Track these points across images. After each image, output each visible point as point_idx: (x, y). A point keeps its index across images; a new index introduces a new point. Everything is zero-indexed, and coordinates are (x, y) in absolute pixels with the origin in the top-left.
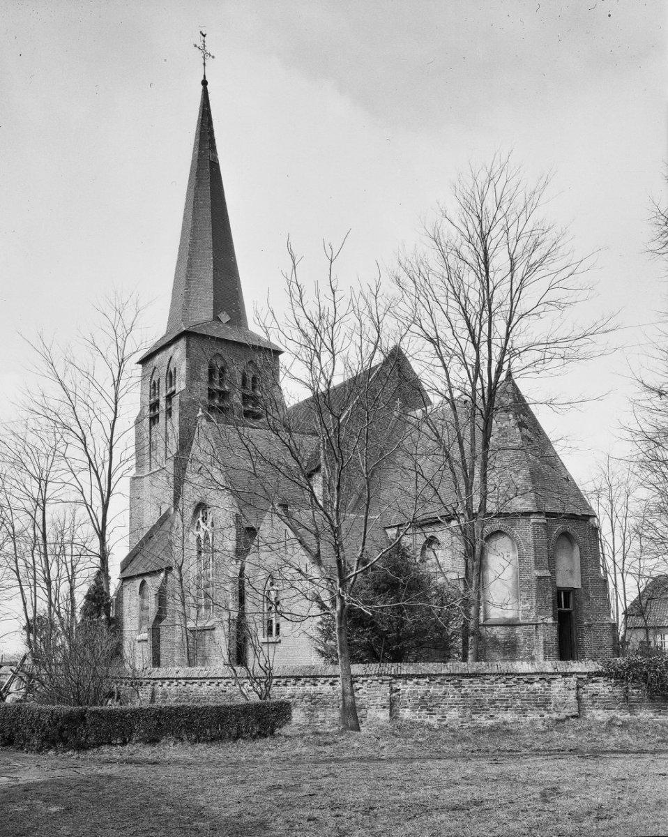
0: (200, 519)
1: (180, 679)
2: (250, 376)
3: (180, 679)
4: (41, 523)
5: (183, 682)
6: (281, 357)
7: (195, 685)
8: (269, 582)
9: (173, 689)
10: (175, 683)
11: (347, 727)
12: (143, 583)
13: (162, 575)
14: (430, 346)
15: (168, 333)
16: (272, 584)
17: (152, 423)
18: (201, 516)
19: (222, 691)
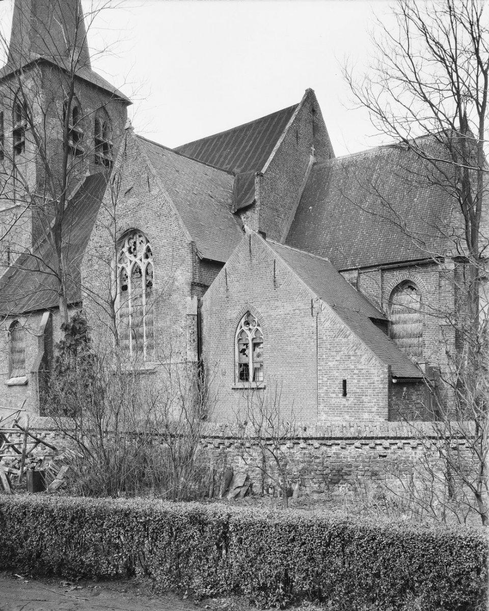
0: (125, 250)
1: (312, 439)
2: (101, 122)
3: (312, 439)
4: (483, 88)
5: (316, 444)
6: (129, 108)
7: (334, 447)
8: (243, 321)
9: (298, 453)
10: (302, 445)
11: (325, 477)
12: (15, 324)
13: (46, 315)
14: (429, 66)
15: (8, 66)
16: (247, 323)
17: (16, 152)
18: (127, 246)
19: (380, 456)
